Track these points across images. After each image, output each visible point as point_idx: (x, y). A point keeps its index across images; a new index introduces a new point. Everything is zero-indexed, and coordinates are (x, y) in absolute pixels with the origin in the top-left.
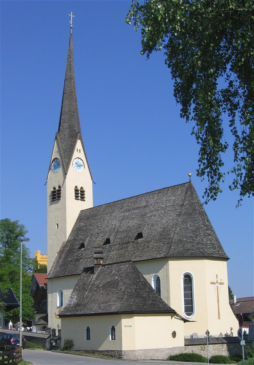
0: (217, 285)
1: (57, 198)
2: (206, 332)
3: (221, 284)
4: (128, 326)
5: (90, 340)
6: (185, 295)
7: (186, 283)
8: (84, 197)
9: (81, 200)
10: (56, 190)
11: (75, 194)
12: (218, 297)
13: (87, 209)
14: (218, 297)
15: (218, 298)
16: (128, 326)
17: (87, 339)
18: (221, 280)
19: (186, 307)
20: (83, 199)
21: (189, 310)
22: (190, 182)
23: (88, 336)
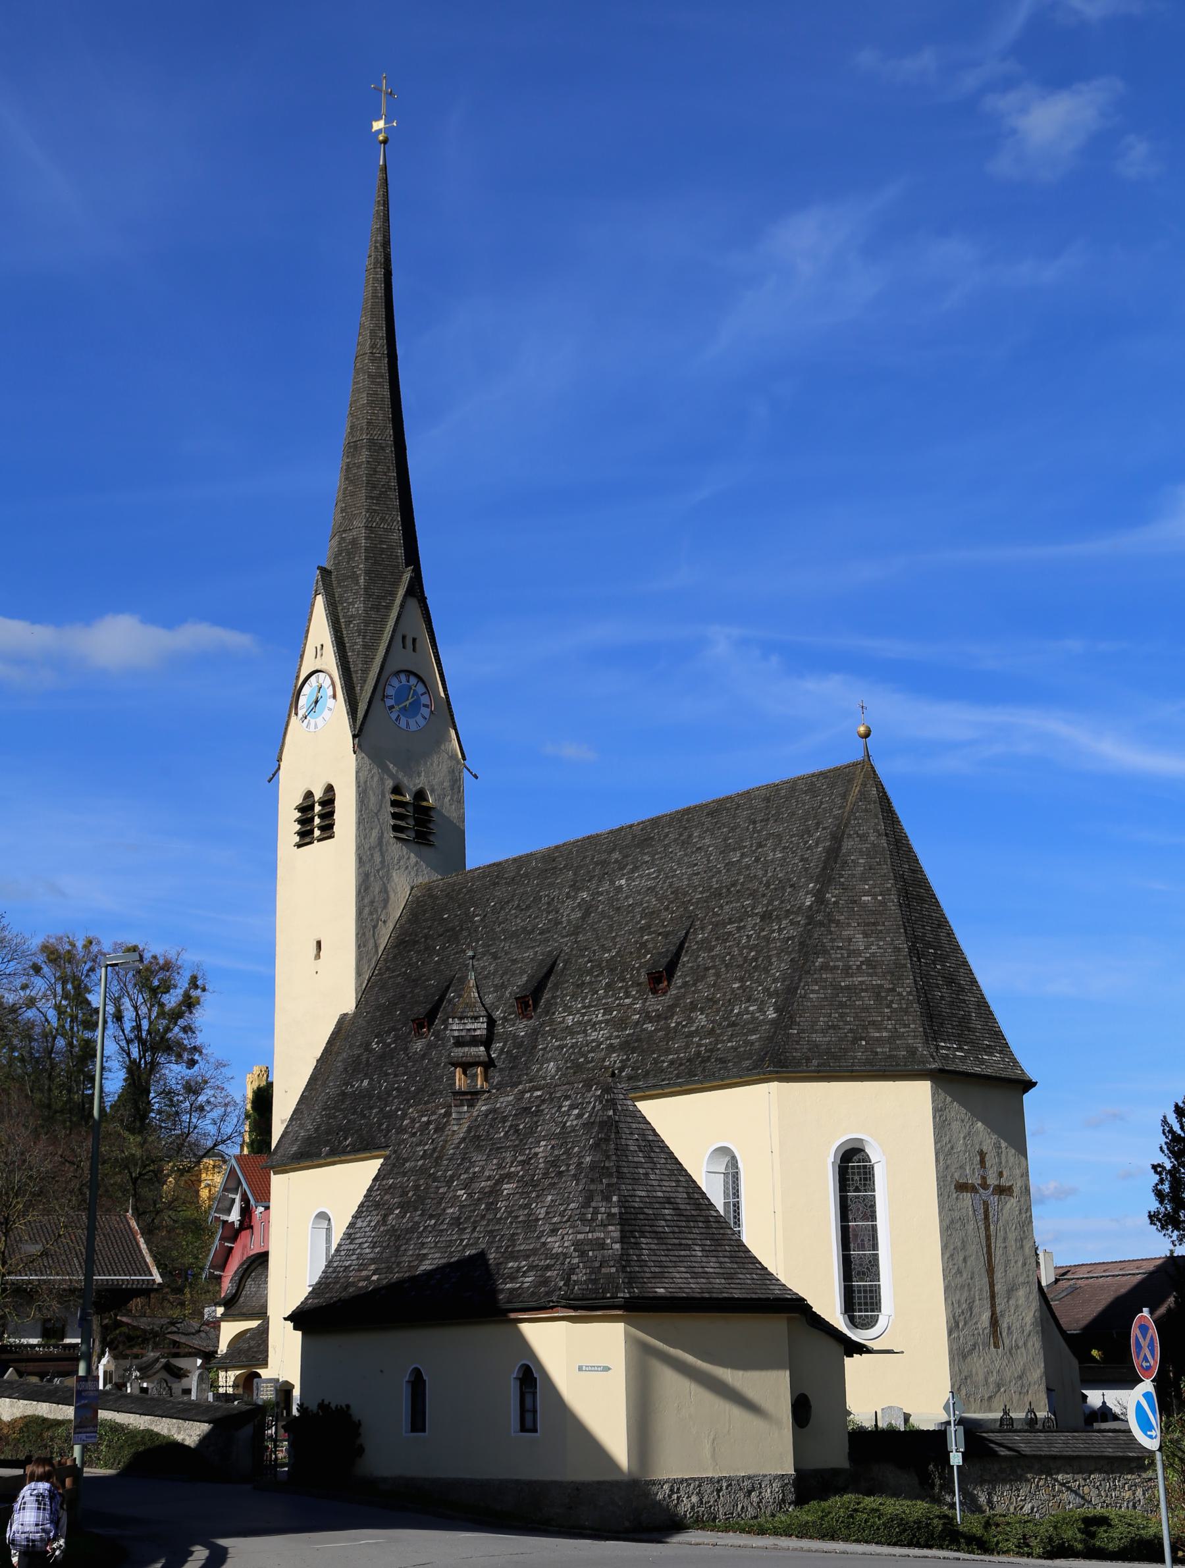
1: (317, 833)
4: (593, 1369)
5: (535, 1431)
6: (872, 1267)
13: (290, 728)
16: (593, 1369)
17: (523, 1429)
21: (866, 1304)
23: (529, 1416)
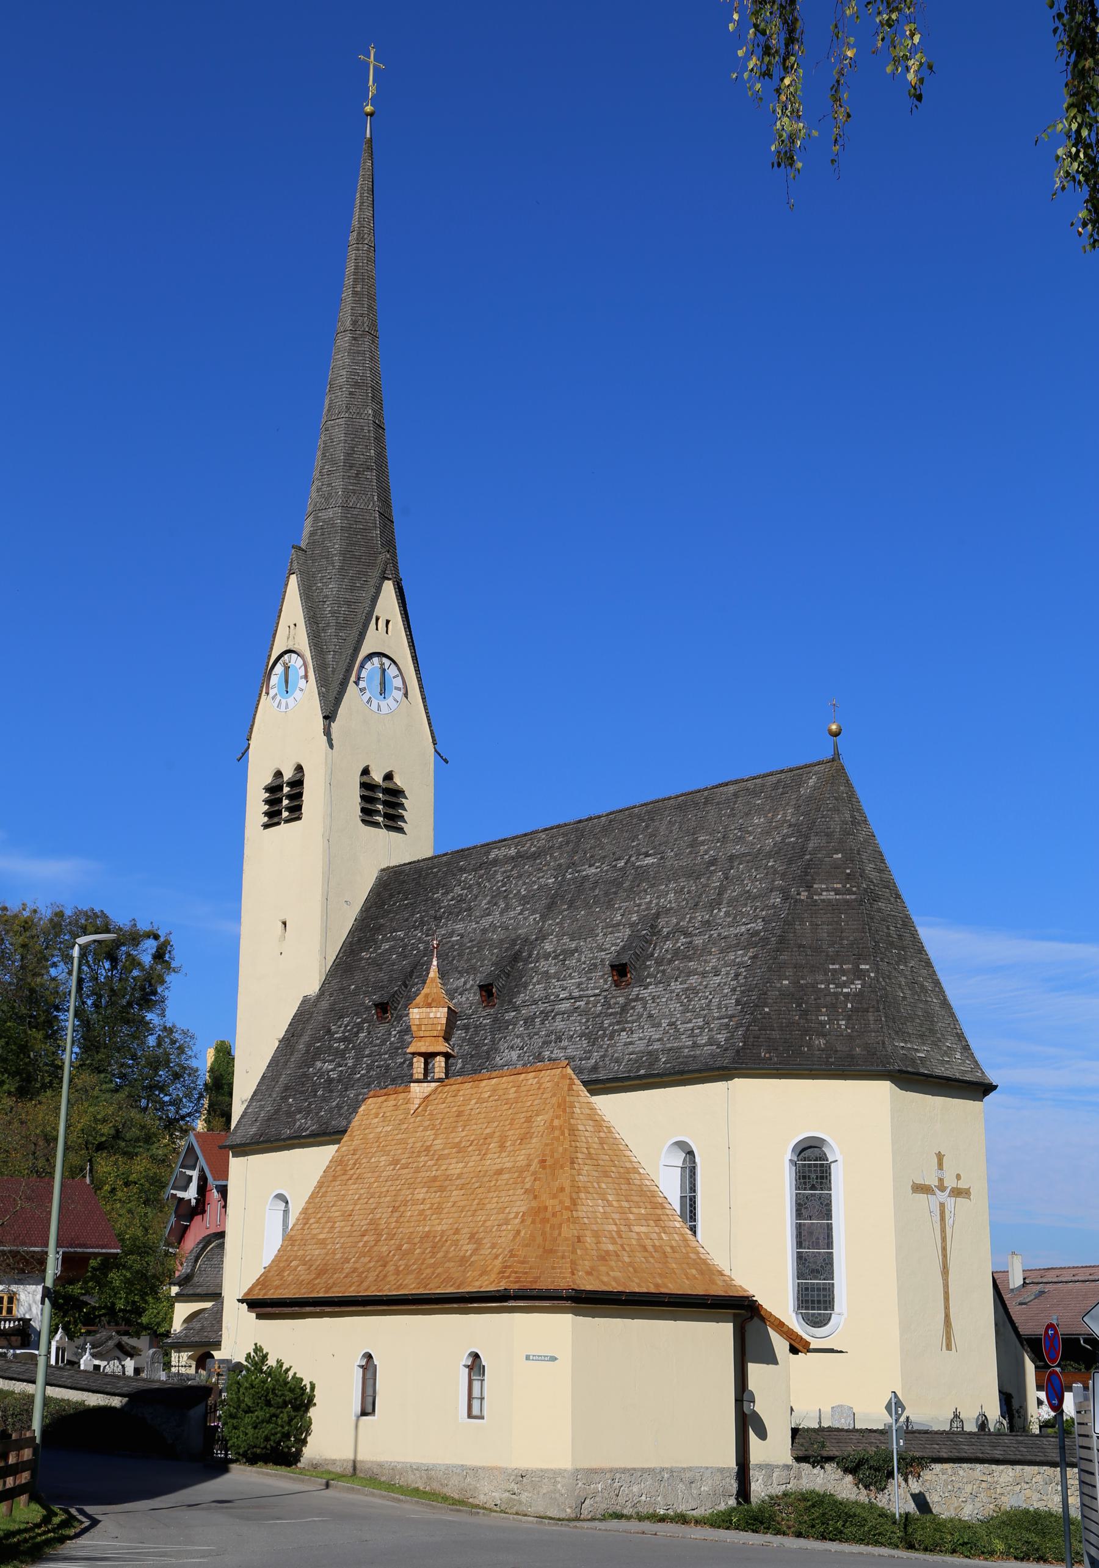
0: (942, 1196)
1: (285, 814)
2: (890, 1403)
3: (957, 1193)
7: (805, 1183)
8: (266, 814)
9: (388, 827)
10: (286, 779)
11: (359, 800)
12: (944, 1249)
14: (944, 1249)
15: (945, 1256)
18: (958, 1177)
19: (807, 1289)
20: (394, 821)
22: (833, 760)
